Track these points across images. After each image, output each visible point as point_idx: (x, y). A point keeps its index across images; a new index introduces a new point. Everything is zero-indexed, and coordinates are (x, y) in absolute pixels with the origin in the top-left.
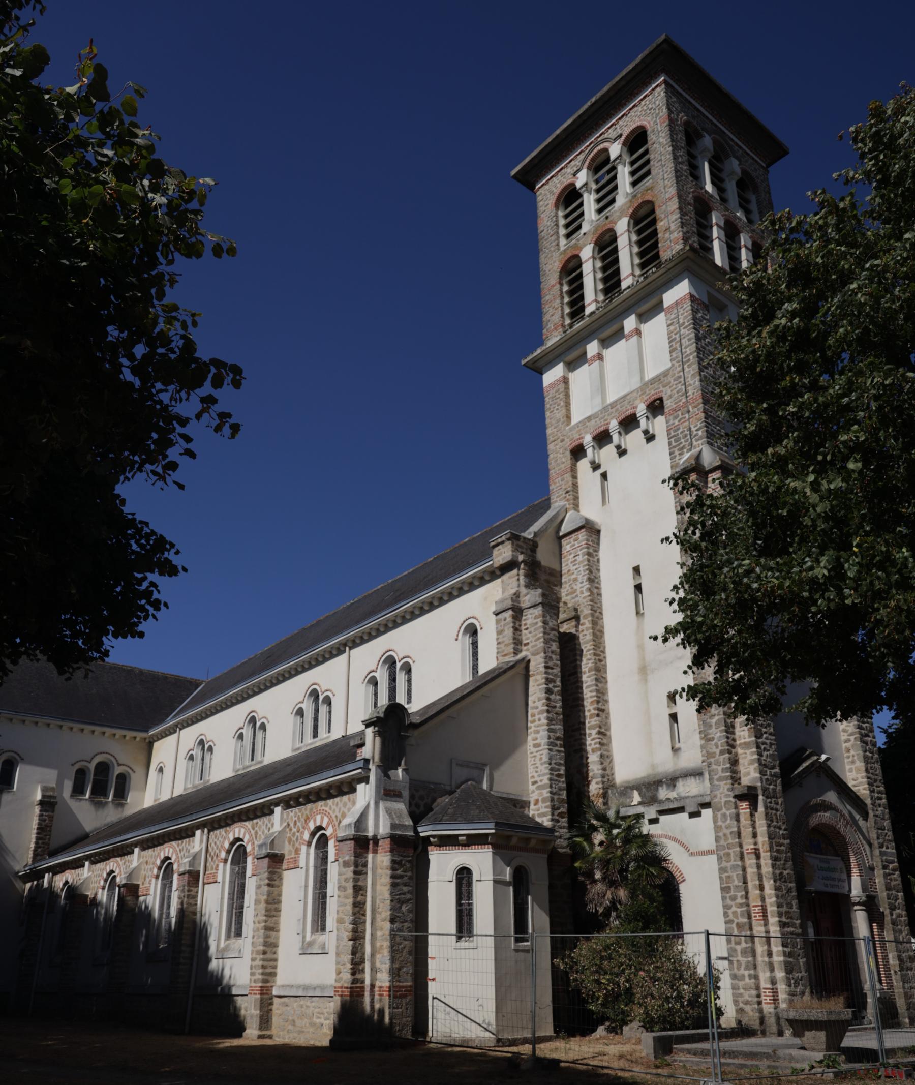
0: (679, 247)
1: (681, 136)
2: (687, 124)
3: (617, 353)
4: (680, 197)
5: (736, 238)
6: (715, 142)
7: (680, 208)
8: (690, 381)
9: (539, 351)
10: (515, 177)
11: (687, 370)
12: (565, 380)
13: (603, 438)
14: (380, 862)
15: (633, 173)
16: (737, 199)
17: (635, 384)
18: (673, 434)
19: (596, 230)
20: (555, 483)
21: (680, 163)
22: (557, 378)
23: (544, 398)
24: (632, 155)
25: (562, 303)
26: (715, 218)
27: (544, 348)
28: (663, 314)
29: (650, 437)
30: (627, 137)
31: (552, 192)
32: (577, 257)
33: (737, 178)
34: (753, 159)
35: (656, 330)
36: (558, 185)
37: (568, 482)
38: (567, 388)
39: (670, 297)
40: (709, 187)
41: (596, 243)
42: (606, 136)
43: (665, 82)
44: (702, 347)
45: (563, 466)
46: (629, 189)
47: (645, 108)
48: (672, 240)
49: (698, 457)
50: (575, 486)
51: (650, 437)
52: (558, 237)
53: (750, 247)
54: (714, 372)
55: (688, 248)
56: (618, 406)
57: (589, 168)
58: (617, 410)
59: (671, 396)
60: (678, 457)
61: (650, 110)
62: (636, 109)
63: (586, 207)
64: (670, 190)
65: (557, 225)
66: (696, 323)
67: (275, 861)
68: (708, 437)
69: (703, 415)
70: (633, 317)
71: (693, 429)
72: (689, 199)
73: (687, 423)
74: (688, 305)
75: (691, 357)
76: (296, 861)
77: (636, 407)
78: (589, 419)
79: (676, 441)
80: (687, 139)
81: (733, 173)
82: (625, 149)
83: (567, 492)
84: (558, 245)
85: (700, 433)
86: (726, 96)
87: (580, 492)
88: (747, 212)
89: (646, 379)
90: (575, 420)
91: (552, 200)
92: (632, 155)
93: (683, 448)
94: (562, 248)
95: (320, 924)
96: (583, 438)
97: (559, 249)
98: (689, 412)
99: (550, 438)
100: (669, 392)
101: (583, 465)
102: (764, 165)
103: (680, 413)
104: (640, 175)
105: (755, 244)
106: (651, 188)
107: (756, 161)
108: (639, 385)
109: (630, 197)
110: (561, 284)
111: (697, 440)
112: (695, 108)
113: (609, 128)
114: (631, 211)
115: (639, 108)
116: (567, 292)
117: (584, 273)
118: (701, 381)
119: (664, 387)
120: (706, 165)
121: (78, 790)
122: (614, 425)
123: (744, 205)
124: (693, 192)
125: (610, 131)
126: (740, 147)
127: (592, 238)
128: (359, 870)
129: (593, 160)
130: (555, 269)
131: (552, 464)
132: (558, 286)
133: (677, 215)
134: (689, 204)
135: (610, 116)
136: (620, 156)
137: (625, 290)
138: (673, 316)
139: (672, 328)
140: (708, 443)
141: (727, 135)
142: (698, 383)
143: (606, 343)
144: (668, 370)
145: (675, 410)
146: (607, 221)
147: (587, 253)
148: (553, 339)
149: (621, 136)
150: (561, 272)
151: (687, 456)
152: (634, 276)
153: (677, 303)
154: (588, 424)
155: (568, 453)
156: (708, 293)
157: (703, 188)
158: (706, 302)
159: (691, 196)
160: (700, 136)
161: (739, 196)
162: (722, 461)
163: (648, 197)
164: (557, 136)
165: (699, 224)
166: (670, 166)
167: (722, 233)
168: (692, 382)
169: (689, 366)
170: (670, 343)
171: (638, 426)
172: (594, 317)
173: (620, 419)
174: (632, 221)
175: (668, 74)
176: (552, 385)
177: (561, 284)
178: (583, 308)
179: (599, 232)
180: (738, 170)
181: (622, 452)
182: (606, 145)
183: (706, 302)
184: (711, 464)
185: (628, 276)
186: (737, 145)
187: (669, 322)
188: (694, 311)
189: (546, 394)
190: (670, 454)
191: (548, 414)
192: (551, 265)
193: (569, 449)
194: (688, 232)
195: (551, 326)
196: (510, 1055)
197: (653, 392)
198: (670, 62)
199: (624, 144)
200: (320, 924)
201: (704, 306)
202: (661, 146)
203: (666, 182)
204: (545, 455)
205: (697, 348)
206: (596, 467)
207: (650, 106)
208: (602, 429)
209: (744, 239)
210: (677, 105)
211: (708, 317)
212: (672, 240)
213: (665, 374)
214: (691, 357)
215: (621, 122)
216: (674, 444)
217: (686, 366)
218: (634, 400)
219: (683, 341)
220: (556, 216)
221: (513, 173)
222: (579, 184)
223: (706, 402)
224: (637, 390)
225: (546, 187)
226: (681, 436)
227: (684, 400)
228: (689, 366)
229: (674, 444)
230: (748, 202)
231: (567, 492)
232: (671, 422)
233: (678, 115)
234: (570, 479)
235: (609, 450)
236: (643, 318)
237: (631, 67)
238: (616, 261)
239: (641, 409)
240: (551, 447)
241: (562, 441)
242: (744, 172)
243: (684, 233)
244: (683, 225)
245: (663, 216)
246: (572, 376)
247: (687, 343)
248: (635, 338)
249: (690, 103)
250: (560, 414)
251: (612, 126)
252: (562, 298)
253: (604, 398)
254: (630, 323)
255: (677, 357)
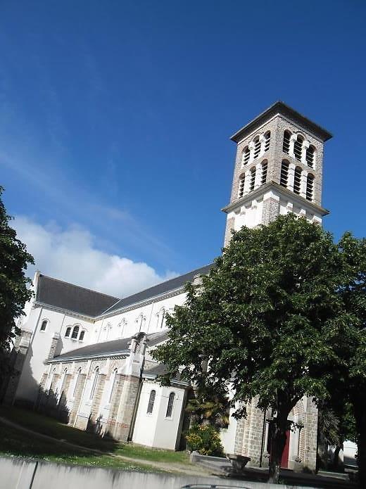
14: (127, 383)
32: (255, 167)
63: (250, 155)
67: (69, 376)
70: (255, 200)
76: (109, 377)
95: (169, 414)
121: (67, 334)
128: (120, 384)
192: (237, 174)
196: (210, 487)
200: (169, 414)
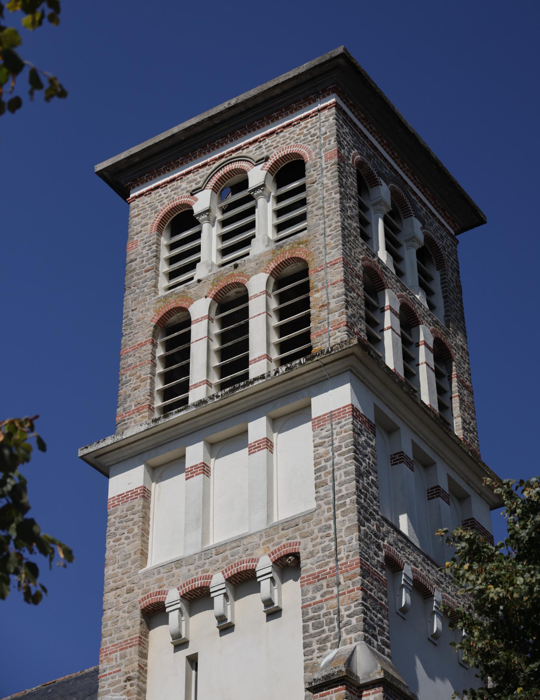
0: (340, 335)
1: (352, 181)
2: (360, 165)
3: (232, 467)
4: (346, 264)
5: (413, 330)
6: (394, 193)
7: (346, 281)
8: (343, 536)
9: (109, 441)
10: (100, 174)
11: (340, 518)
12: (145, 494)
13: (197, 598)
15: (279, 213)
16: (416, 274)
17: (258, 523)
18: (311, 614)
19: (218, 279)
20: (109, 660)
21: (349, 217)
22: (133, 487)
23: (106, 515)
24: (279, 187)
25: (153, 374)
26: (390, 299)
27: (119, 438)
28: (309, 425)
29: (273, 612)
30: (276, 163)
31: (154, 208)
33: (418, 246)
34: (440, 222)
35: (297, 445)
36: (166, 201)
37: (131, 662)
38: (146, 507)
39: (324, 403)
40: (383, 255)
41: (215, 298)
42: (244, 152)
43: (336, 105)
44: (364, 487)
45: (126, 633)
46: (272, 234)
47: (305, 131)
48: (330, 323)
49: (349, 661)
50: (143, 669)
51: (273, 612)
52: (158, 275)
53: (397, 309)
54: (378, 527)
55: (355, 342)
56: (228, 553)
57: (215, 189)
58: (225, 558)
59: (312, 554)
60: (316, 654)
61: (314, 133)
62: (292, 129)
64: (334, 252)
65: (157, 257)
66: (358, 451)
68: (365, 631)
69: (360, 593)
71: (344, 613)
72: (357, 269)
73: (335, 601)
74: (347, 422)
75: (348, 501)
77: (257, 560)
78: (178, 563)
79: (315, 627)
80: (360, 182)
81: (413, 238)
82: (271, 178)
83: (129, 679)
84: (155, 286)
85: (354, 621)
86: (413, 137)
87: (148, 681)
88: (429, 293)
89: (275, 520)
90: (154, 559)
91: (154, 220)
92: (279, 187)
93: (326, 639)
94: (162, 293)
96: (165, 593)
97: (156, 293)
98: (338, 584)
99: (109, 584)
100: (310, 548)
101: (160, 637)
102: (453, 233)
103: (324, 583)
104: (290, 218)
105: (437, 341)
106: (306, 243)
107: (443, 225)
108: (263, 526)
109: (273, 246)
110: (154, 345)
111: (348, 632)
112: (372, 145)
113: (250, 143)
114: (273, 266)
115: (297, 130)
116: (162, 358)
117: (193, 338)
118: (360, 540)
119: (304, 537)
120: (381, 223)
122: (218, 581)
123: (424, 284)
124: (363, 260)
125: (251, 148)
126: (425, 205)
127: (206, 288)
129: (222, 180)
130: (148, 320)
131: (107, 626)
132: (149, 347)
133: (340, 289)
134: (358, 276)
135: (252, 128)
136: (263, 185)
137: (255, 379)
138: (324, 433)
139: (321, 450)
140: (365, 639)
141: (407, 179)
142: (355, 543)
143: (217, 448)
144: (312, 512)
145: (317, 577)
146: (236, 272)
147: (200, 308)
148: (135, 426)
149: (267, 159)
150: (155, 327)
151: (331, 654)
152: (270, 359)
153: (331, 415)
154: (175, 571)
155: (137, 613)
156: (377, 409)
157: (375, 255)
158: (373, 422)
159: (360, 264)
160: (377, 184)
161: (420, 271)
162: (386, 672)
163: (298, 254)
164: (173, 136)
165: (368, 304)
166: (335, 219)
167: (397, 321)
168: (346, 539)
169: (344, 514)
170: (316, 472)
171: (258, 590)
172: (203, 409)
173: (229, 573)
174: (273, 280)
175: (341, 94)
176: (123, 498)
177: (154, 345)
178: (185, 387)
179: (222, 284)
180: (421, 237)
181: (226, 627)
182: (244, 165)
183: (373, 422)
184: (368, 674)
185: (260, 358)
186: (421, 201)
187: (318, 441)
188: (357, 433)
189: (110, 510)
190: (305, 646)
191: (110, 543)
192: (142, 313)
193: (139, 607)
194: (353, 315)
195: (131, 405)
197: (284, 542)
198: (343, 80)
199: (270, 171)
201: (371, 425)
202: (323, 185)
203: (328, 239)
204: (98, 611)
205: (357, 488)
206: (180, 643)
207: (313, 131)
208: (198, 584)
209: (424, 334)
210: (349, 138)
211: (373, 443)
212: (330, 323)
213: (307, 517)
214: (348, 501)
215: (268, 140)
216: (311, 631)
217: (338, 512)
218: (253, 548)
219: (337, 473)
220: (158, 244)
221: (99, 167)
222: (197, 208)
223: (365, 573)
224: (260, 534)
225: (146, 199)
226: (323, 619)
227: (332, 565)
228: (344, 514)
229: (311, 631)
230: (429, 278)
231: (129, 679)
232: (310, 595)
233: (349, 152)
234: (136, 657)
235: (203, 623)
236: (279, 423)
237: (291, 74)
238: (245, 329)
239: (264, 565)
240: (109, 597)
241: (130, 591)
242: (427, 238)
243: (349, 317)
244: (348, 304)
245: (320, 285)
246: (155, 488)
247: (343, 478)
248: (264, 452)
249: (366, 137)
250: (130, 547)
251: (255, 141)
252: (154, 365)
253: (205, 536)
254: (258, 428)
255: (326, 496)
